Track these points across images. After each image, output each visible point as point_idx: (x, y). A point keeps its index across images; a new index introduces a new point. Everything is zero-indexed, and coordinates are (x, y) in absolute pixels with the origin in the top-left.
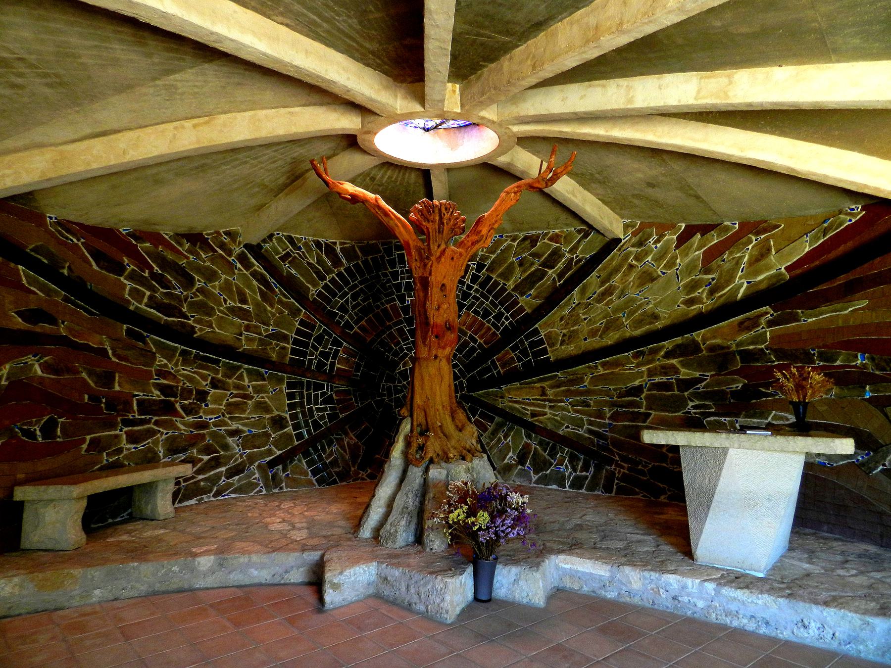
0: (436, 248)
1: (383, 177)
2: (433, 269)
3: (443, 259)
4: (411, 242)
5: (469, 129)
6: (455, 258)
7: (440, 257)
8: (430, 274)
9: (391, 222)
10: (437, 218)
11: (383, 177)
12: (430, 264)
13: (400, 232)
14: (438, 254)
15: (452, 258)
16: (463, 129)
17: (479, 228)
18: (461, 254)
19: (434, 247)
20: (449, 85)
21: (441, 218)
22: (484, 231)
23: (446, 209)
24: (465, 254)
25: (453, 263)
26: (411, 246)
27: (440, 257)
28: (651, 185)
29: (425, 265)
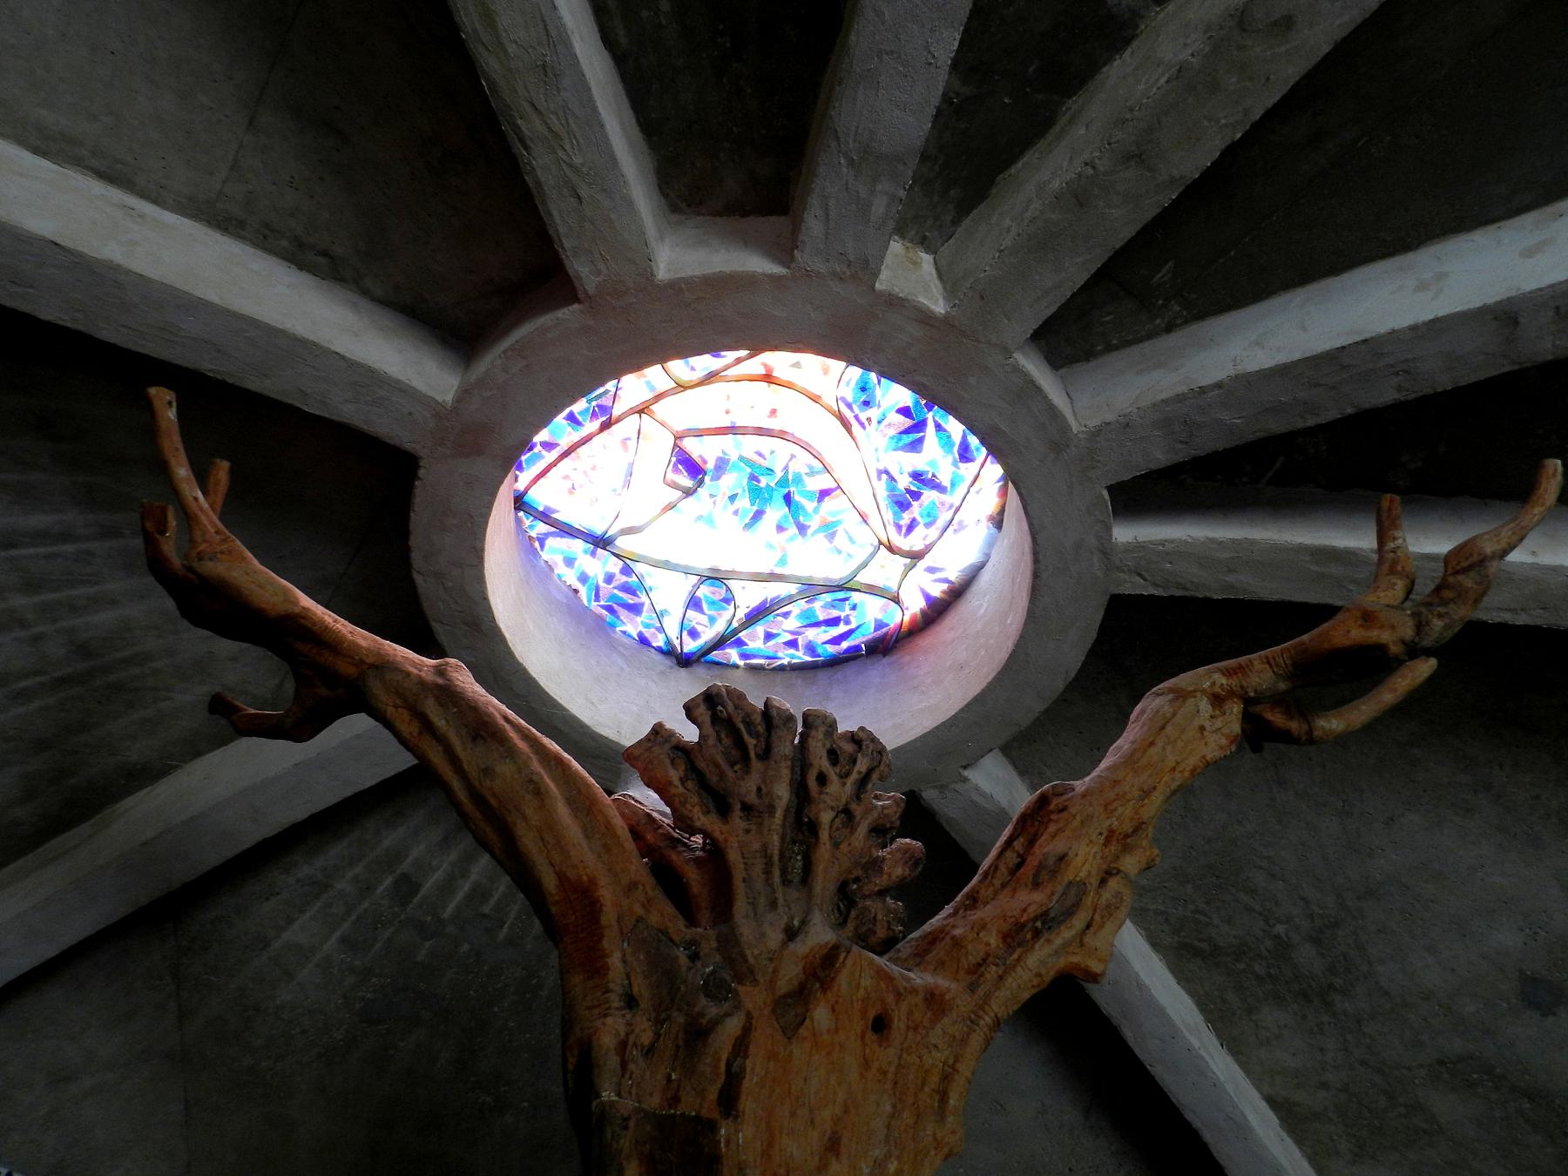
0: (774, 937)
1: (447, 887)
2: (755, 1066)
3: (821, 1015)
4: (607, 894)
5: (849, 670)
6: (898, 1023)
7: (801, 996)
8: (729, 1100)
9: (505, 769)
10: (783, 792)
11: (447, 887)
12: (733, 1026)
13: (549, 826)
14: (790, 974)
15: (880, 1025)
16: (822, 675)
17: (1048, 847)
18: (935, 1002)
19: (758, 932)
20: (896, 246)
21: (801, 794)
22: (1085, 859)
23: (833, 755)
24: (964, 1003)
25: (886, 1056)
26: (609, 916)
27: (801, 996)
28: (1539, 994)
29: (697, 1034)
